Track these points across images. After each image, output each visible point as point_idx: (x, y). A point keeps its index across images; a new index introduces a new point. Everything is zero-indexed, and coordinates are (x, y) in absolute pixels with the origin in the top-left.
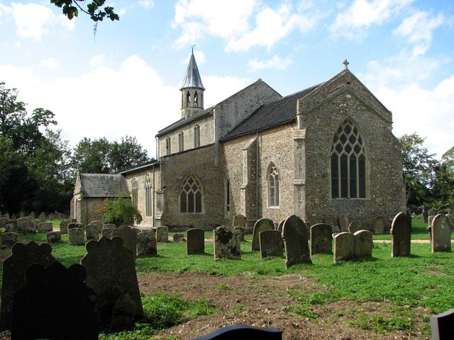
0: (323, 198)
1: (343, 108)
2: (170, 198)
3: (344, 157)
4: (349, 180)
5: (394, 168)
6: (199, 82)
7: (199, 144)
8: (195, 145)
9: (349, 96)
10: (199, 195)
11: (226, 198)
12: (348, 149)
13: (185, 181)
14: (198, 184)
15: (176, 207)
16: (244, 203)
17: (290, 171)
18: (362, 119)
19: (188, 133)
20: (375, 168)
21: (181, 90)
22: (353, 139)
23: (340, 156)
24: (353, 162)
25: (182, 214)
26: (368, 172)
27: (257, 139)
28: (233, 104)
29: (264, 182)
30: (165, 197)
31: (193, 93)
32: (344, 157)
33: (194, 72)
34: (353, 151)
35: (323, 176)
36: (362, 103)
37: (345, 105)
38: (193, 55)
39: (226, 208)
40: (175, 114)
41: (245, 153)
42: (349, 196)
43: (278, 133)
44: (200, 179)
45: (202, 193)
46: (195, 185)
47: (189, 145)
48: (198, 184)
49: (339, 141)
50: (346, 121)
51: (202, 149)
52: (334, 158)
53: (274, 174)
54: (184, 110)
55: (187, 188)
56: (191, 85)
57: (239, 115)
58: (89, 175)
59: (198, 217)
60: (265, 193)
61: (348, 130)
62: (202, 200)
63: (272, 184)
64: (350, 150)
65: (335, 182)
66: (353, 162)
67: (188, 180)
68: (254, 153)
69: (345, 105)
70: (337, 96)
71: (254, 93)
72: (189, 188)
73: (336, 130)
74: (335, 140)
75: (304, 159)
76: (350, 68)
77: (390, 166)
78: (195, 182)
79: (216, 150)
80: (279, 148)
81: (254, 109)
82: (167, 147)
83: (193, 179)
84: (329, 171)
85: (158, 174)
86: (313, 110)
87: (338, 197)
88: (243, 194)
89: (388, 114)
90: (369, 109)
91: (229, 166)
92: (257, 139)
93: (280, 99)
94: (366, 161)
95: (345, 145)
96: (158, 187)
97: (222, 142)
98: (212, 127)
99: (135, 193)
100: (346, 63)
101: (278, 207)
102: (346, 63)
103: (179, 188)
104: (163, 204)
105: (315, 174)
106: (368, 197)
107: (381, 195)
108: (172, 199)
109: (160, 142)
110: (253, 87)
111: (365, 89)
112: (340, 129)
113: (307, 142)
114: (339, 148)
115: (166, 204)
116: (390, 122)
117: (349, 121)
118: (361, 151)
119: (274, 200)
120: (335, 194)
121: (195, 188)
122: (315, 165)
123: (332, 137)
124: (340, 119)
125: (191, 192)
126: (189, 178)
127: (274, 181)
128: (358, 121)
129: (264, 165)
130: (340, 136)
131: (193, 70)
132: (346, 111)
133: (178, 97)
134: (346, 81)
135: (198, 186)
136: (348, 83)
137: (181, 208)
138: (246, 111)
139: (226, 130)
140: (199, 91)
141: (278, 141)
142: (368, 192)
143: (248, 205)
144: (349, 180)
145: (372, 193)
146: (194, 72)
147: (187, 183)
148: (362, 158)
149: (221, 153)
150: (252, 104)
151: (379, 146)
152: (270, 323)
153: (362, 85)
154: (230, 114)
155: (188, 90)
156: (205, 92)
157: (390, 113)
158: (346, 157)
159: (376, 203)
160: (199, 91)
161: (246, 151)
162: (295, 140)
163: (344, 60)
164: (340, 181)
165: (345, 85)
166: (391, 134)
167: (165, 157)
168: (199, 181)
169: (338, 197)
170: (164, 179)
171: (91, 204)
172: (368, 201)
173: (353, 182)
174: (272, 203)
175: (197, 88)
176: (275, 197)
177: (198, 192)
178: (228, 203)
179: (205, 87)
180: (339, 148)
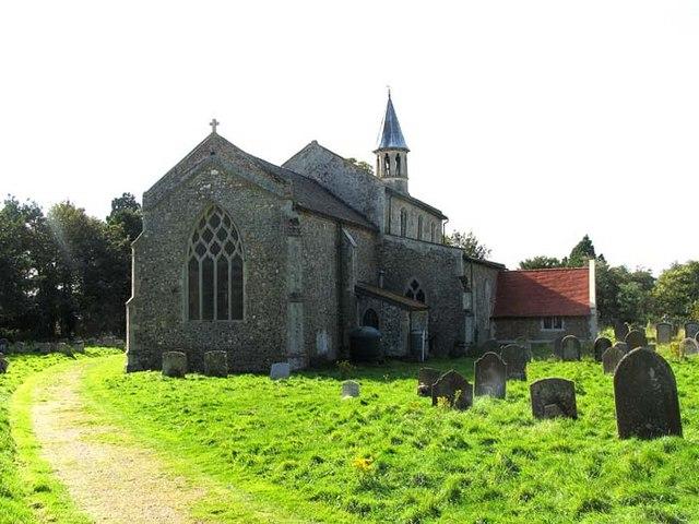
9: (214, 172)
21: (375, 152)
24: (223, 277)
42: (230, 318)
52: (193, 264)
58: (245, 279)
66: (223, 277)
73: (197, 224)
76: (220, 132)
112: (203, 223)
120: (193, 314)
128: (228, 206)
156: (409, 155)
159: (256, 327)
179: (409, 146)
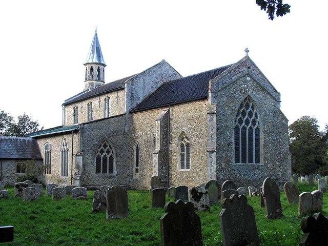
0: (228, 163)
2: (88, 161)
3: (244, 128)
4: (247, 148)
5: (282, 139)
6: (102, 59)
9: (248, 79)
10: (111, 158)
11: (135, 160)
12: (247, 122)
13: (101, 146)
15: (92, 169)
16: (157, 166)
17: (201, 140)
18: (258, 97)
20: (267, 138)
22: (250, 114)
23: (241, 127)
24: (251, 134)
25: (97, 175)
26: (262, 142)
27: (169, 111)
29: (175, 147)
30: (83, 159)
31: (96, 69)
32: (244, 128)
33: (97, 49)
34: (244, 123)
37: (246, 86)
38: (96, 34)
39: (134, 170)
40: (79, 86)
41: (158, 123)
44: (114, 144)
45: (114, 156)
46: (108, 150)
47: (98, 115)
49: (240, 116)
50: (246, 99)
51: (116, 119)
52: (237, 128)
54: (87, 82)
55: (102, 152)
56: (94, 61)
59: (111, 177)
60: (176, 158)
61: (247, 106)
62: (114, 163)
63: (183, 150)
64: (246, 121)
65: (237, 150)
66: (251, 134)
68: (166, 123)
69: (246, 86)
70: (239, 79)
74: (237, 115)
75: (215, 130)
77: (278, 137)
78: (108, 147)
80: (190, 120)
82: (74, 115)
84: (233, 140)
85: (77, 137)
86: (222, 89)
87: (106, 173)
88: (156, 158)
89: (277, 94)
90: (264, 90)
91: (138, 133)
92: (169, 111)
93: (179, 77)
94: (260, 133)
95: (245, 119)
96: (76, 150)
97: (132, 112)
98: (123, 99)
99: (48, 154)
100: (247, 51)
101: (188, 170)
102: (247, 51)
104: (81, 165)
105: (223, 143)
106: (262, 162)
107: (272, 161)
108: (89, 161)
109: (66, 109)
111: (261, 73)
112: (241, 106)
113: (219, 114)
114: (240, 121)
115: (84, 165)
116: (278, 101)
117: (248, 98)
118: (257, 124)
119: (184, 163)
120: (237, 160)
121: (108, 152)
122: (222, 135)
123: (236, 113)
124: (242, 97)
125: (105, 155)
126: (104, 143)
127: (185, 149)
128: (255, 99)
129: (175, 134)
130: (241, 111)
133: (82, 72)
134: (247, 64)
136: (249, 68)
138: (152, 87)
140: (101, 67)
141: (189, 114)
142: (262, 159)
144: (247, 148)
145: (265, 159)
146: (97, 49)
147: (102, 147)
148: (258, 129)
149: (131, 121)
150: (157, 81)
153: (259, 70)
155: (91, 65)
157: (279, 94)
158: (245, 129)
160: (101, 67)
161: (159, 122)
162: (208, 114)
164: (241, 149)
165: (246, 69)
166: (280, 111)
167: (84, 124)
169: (106, 173)
170: (83, 143)
173: (251, 150)
174: (182, 167)
175: (100, 64)
177: (111, 156)
178: (137, 166)
180: (240, 121)
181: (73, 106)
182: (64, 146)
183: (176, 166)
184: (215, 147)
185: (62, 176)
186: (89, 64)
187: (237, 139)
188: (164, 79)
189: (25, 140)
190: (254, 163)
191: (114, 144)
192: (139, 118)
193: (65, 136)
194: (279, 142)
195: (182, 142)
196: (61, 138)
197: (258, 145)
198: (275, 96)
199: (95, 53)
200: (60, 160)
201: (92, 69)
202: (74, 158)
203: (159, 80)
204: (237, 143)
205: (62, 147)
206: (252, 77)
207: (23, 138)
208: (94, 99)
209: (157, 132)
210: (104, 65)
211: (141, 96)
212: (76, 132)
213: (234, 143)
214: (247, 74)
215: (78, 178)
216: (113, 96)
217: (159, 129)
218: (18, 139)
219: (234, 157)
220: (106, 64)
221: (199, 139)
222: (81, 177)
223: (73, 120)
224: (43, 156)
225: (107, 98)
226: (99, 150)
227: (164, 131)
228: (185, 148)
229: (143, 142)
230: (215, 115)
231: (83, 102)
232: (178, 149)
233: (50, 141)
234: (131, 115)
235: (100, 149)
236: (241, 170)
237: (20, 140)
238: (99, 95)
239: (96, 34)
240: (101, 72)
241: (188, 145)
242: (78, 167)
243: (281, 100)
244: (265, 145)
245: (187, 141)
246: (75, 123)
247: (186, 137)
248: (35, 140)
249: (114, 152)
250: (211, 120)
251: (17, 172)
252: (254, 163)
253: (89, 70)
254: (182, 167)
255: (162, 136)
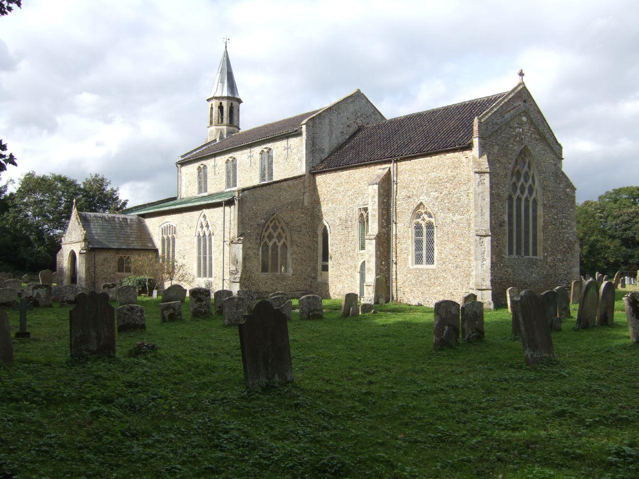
1: (519, 134)
5: (566, 218)
7: (271, 175)
8: (263, 177)
9: (524, 119)
14: (284, 232)
15: (256, 265)
17: (457, 217)
18: (537, 149)
19: (217, 166)
26: (540, 222)
28: (327, 121)
35: (501, 226)
36: (540, 134)
37: (521, 130)
39: (320, 267)
43: (357, 170)
44: (287, 224)
45: (288, 244)
48: (284, 232)
51: (290, 182)
52: (510, 198)
53: (424, 220)
55: (270, 237)
56: (225, 94)
57: (334, 136)
65: (511, 231)
67: (271, 225)
68: (386, 187)
69: (521, 130)
71: (352, 108)
72: (273, 237)
75: (488, 199)
79: (307, 181)
80: (437, 183)
81: (352, 130)
83: (277, 224)
84: (506, 219)
85: (232, 212)
95: (520, 184)
97: (314, 172)
99: (169, 242)
100: (521, 74)
102: (521, 74)
103: (260, 237)
106: (540, 256)
110: (350, 100)
118: (534, 193)
120: (511, 253)
121: (279, 237)
124: (517, 148)
125: (275, 243)
126: (272, 220)
131: (228, 72)
132: (522, 139)
135: (284, 235)
137: (262, 269)
138: (342, 133)
139: (320, 156)
140: (235, 103)
141: (433, 175)
142: (540, 248)
143: (379, 263)
145: (545, 249)
148: (535, 201)
150: (349, 122)
151: (550, 189)
152: (593, 444)
154: (324, 135)
160: (235, 103)
162: (476, 172)
163: (518, 71)
166: (563, 173)
168: (285, 227)
170: (242, 222)
171: (100, 257)
172: (541, 260)
173: (527, 233)
176: (424, 252)
181: (196, 165)
182: (202, 227)
183: (406, 260)
184: (487, 226)
185: (199, 276)
186: (216, 98)
187: (510, 216)
188: (358, 121)
189: (126, 219)
190: (531, 256)
191: (287, 224)
192: (326, 183)
193: (206, 211)
194: (561, 223)
195: (419, 220)
196: (196, 214)
197: (535, 227)
198: (556, 150)
199: (226, 81)
200: (195, 251)
201: (221, 108)
202: (227, 248)
203: (352, 122)
204: (510, 224)
205: (199, 229)
206: (528, 117)
207: (122, 216)
208: (240, 152)
209: (370, 203)
210: (240, 101)
211: (327, 144)
212: (230, 203)
213: (507, 222)
214: (523, 112)
215: (238, 280)
216: (278, 148)
217: (376, 199)
218: (114, 217)
219: (507, 245)
220: (242, 100)
221: (454, 215)
222: (241, 278)
223: (196, 186)
224: (158, 244)
225: (265, 150)
226: (266, 234)
227: (383, 202)
228: (425, 230)
229: (338, 222)
230: (487, 175)
231: (218, 158)
232: (411, 232)
233: (171, 219)
234: (312, 176)
235: (268, 232)
236: (516, 266)
237: (118, 218)
238: (214, 156)
239: (226, 54)
240: (235, 111)
241: (430, 226)
242: (235, 262)
243: (563, 157)
244: (545, 228)
245: (427, 219)
246: (200, 192)
247: (426, 213)
248: (141, 218)
249: (289, 238)
250: (481, 183)
251: (119, 271)
252: (531, 256)
253: (217, 109)
254: (418, 260)
255: (381, 211)
